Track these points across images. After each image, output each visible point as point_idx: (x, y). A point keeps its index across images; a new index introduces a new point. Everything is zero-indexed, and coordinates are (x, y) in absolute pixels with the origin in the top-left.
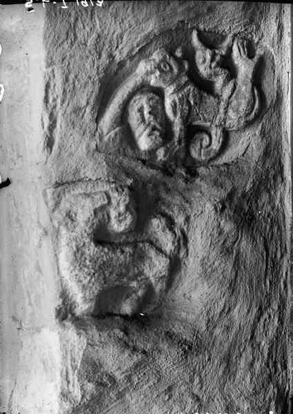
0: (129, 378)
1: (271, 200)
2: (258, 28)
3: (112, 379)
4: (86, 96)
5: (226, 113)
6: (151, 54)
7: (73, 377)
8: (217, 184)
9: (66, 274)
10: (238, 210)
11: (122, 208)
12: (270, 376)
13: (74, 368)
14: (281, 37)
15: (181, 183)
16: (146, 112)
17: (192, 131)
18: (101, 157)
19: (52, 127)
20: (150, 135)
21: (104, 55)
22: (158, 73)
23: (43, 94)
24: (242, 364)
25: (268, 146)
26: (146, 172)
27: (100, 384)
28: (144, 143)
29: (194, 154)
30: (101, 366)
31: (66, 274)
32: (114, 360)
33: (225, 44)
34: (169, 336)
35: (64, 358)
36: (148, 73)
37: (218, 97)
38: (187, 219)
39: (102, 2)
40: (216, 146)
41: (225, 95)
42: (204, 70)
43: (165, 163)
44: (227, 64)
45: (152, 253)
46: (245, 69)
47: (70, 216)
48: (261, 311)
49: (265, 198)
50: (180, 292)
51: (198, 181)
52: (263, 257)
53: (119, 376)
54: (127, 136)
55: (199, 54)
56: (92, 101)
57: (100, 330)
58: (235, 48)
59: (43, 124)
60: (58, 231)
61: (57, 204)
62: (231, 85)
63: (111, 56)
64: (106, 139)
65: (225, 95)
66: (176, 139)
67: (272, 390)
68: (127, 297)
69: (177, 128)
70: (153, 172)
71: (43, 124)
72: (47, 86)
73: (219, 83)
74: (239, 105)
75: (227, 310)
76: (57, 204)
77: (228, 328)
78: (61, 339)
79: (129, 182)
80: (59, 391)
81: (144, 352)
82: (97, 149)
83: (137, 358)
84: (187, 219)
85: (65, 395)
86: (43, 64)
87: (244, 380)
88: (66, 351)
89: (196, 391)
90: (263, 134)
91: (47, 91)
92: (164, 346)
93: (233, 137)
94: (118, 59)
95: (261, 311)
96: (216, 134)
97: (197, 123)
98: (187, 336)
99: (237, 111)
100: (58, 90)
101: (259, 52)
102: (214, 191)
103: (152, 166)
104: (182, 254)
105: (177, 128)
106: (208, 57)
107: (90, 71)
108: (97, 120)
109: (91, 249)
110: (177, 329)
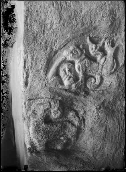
4: (41, 65)
5: (102, 69)
28: (66, 83)
29: (88, 86)
38: (85, 112)
40: (97, 83)
63: (52, 49)
66: (80, 81)
74: (107, 66)
84: (85, 112)
91: (25, 63)
96: (98, 78)
110: (80, 156)
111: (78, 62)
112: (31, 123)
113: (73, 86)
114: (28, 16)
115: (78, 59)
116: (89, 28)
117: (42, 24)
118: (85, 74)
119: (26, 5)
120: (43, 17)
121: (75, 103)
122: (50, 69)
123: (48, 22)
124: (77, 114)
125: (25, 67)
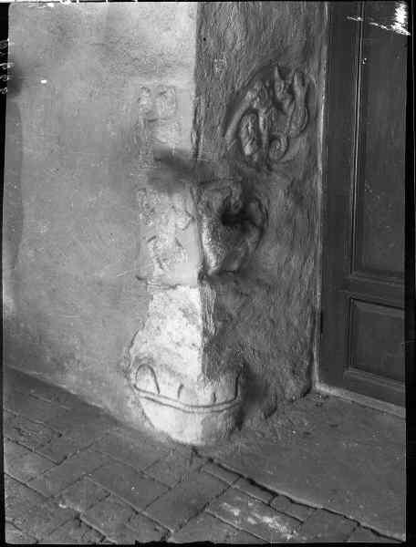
0: (239, 314)
1: (311, 185)
2: (308, 65)
3: (230, 316)
4: (218, 117)
5: (290, 126)
6: (254, 85)
7: (210, 319)
8: (285, 176)
9: (207, 248)
10: (296, 193)
11: (237, 198)
12: (309, 300)
13: (210, 313)
14: (320, 69)
15: (265, 177)
16: (249, 128)
17: (272, 139)
18: (225, 161)
19: (198, 141)
20: (252, 144)
21: (229, 87)
22: (258, 99)
23: (193, 117)
24: (295, 294)
25: (311, 147)
26: (248, 171)
27: (225, 321)
28: (248, 150)
29: (271, 155)
30: (224, 309)
31: (207, 248)
32: (231, 303)
33: (291, 75)
34: (258, 282)
35: (204, 307)
36: (253, 100)
37: (285, 114)
38: (269, 202)
39: (184, 18)
40: (283, 150)
41: (290, 114)
42: (279, 95)
43: (257, 164)
44: (291, 91)
45: (250, 227)
46: (299, 92)
47: (208, 205)
48: (305, 259)
49: (308, 182)
50: (48, 359)
51: (274, 174)
52: (312, 226)
53: (234, 313)
54: (239, 147)
55: (277, 84)
56: (222, 121)
57: (223, 284)
58: (296, 79)
59: (192, 140)
60: (201, 217)
61: (200, 199)
62: (293, 106)
63: (233, 88)
64: (228, 149)
65: (290, 114)
66: (264, 146)
67: (309, 309)
68: (234, 259)
69: (265, 139)
70: (251, 170)
71: (192, 140)
72: (196, 111)
73: (287, 103)
74: (297, 120)
75: (288, 260)
76: (200, 199)
77: (289, 273)
78: (201, 293)
79: (240, 179)
80: (202, 330)
81: (247, 295)
82: (224, 157)
83: (245, 298)
84: (269, 202)
85: (205, 333)
86: (193, 94)
87: (296, 306)
88: (204, 301)
89: (272, 316)
90: (308, 139)
91: (195, 115)
92: (257, 289)
93: (292, 141)
94: (236, 88)
95: (305, 259)
96: (283, 140)
97: (274, 133)
98: (269, 282)
99: (296, 124)
100: (202, 113)
101: (307, 81)
102: (285, 181)
103: (251, 166)
104: (265, 225)
105: (265, 139)
106: (283, 86)
107: (222, 97)
108: (224, 135)
109: (221, 229)
110: (262, 276)
111: (264, 111)
112: (205, 225)
113: (256, 158)
114: (202, 23)
115: (249, 231)
116: (302, 340)
117: (220, 41)
118: (270, 131)
119: (244, 12)
120: (223, 26)
121: (257, 187)
122: (234, 113)
123: (229, 35)
124: (260, 206)
125: (195, 121)
